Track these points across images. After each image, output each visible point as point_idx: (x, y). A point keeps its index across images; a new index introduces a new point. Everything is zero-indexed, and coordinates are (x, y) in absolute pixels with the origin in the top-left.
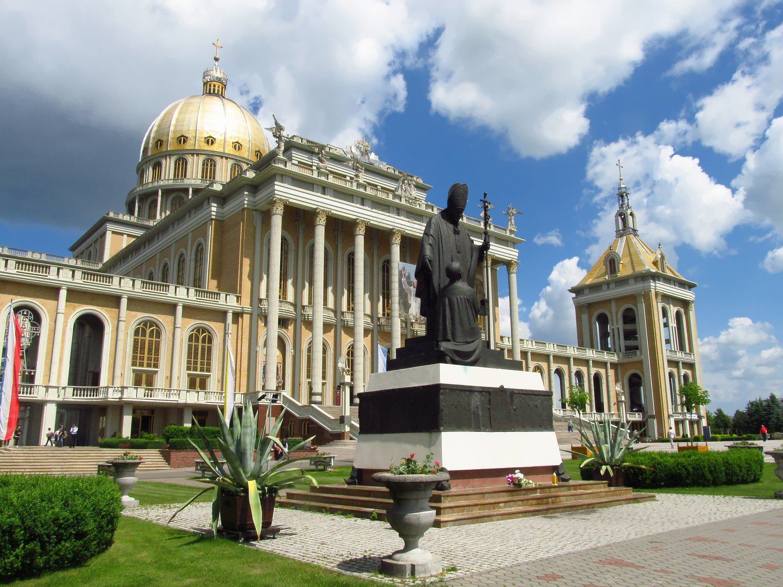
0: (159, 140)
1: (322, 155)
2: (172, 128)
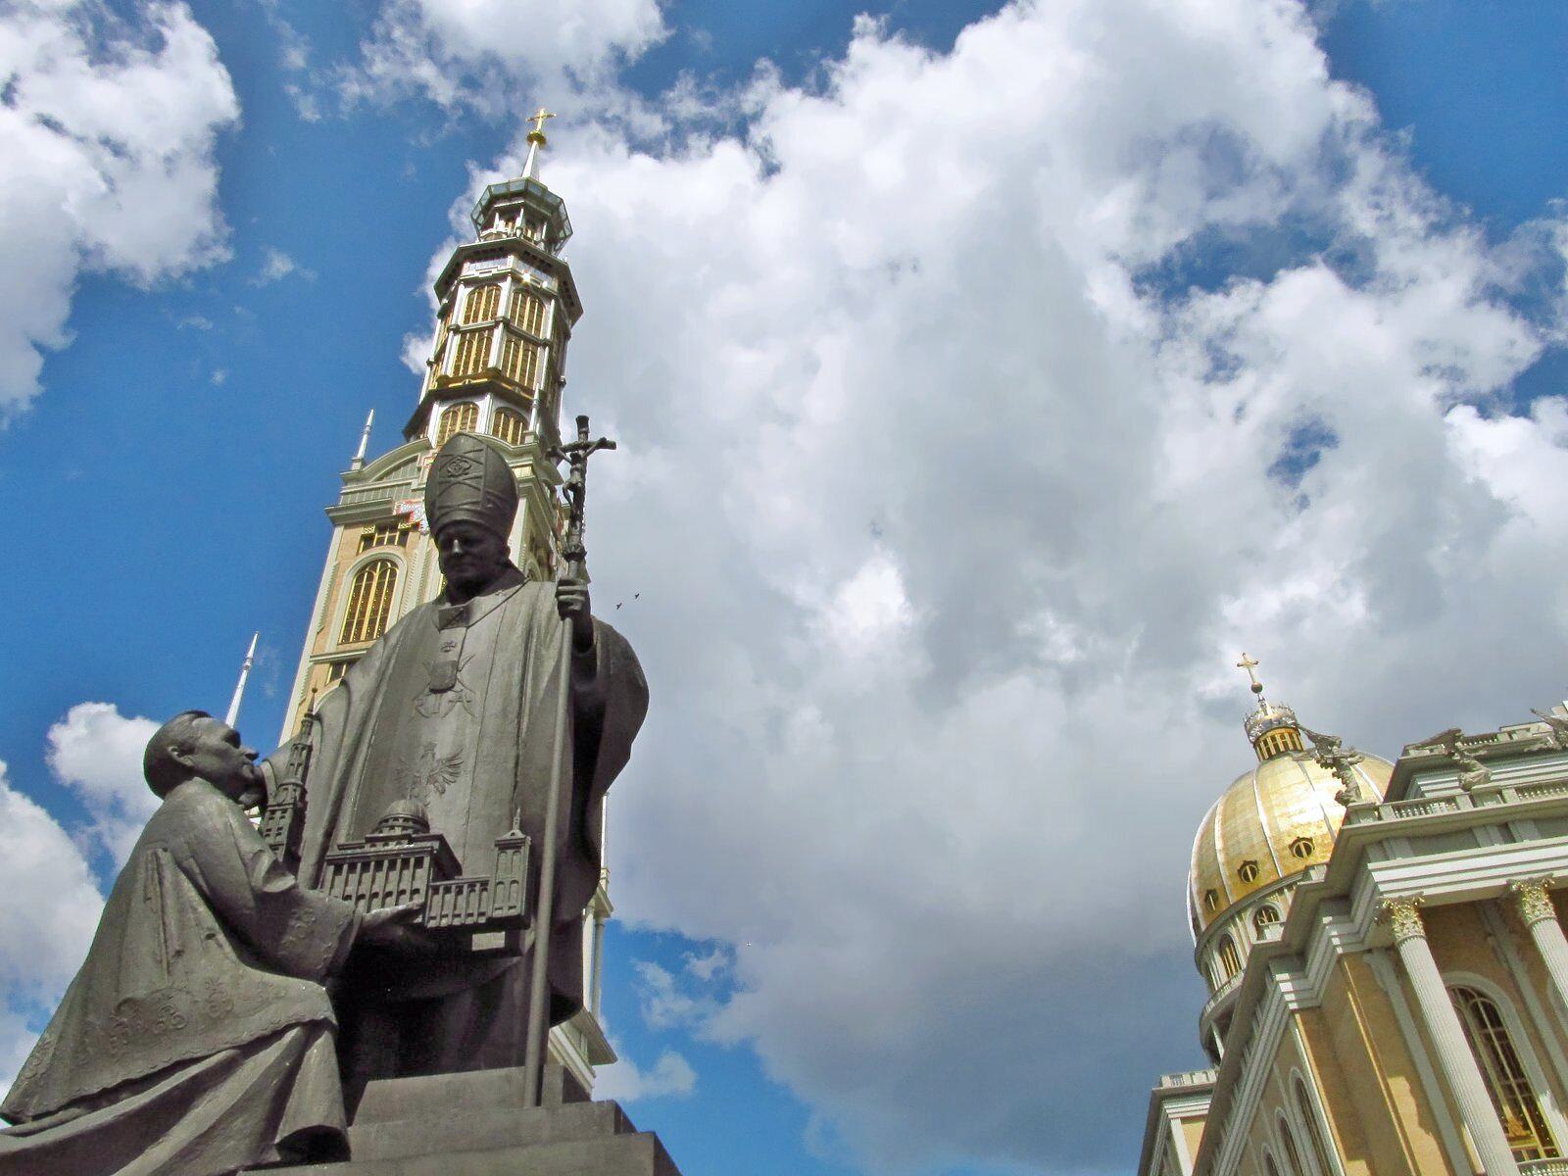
0: (1209, 892)
1: (1462, 754)
2: (1221, 858)
